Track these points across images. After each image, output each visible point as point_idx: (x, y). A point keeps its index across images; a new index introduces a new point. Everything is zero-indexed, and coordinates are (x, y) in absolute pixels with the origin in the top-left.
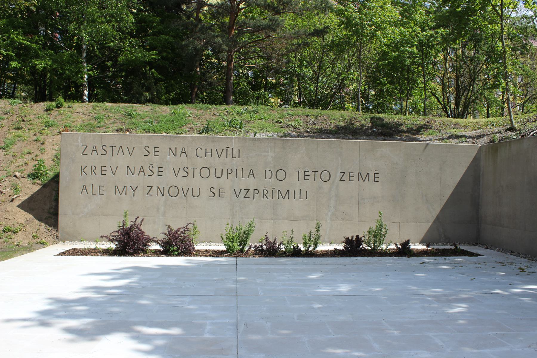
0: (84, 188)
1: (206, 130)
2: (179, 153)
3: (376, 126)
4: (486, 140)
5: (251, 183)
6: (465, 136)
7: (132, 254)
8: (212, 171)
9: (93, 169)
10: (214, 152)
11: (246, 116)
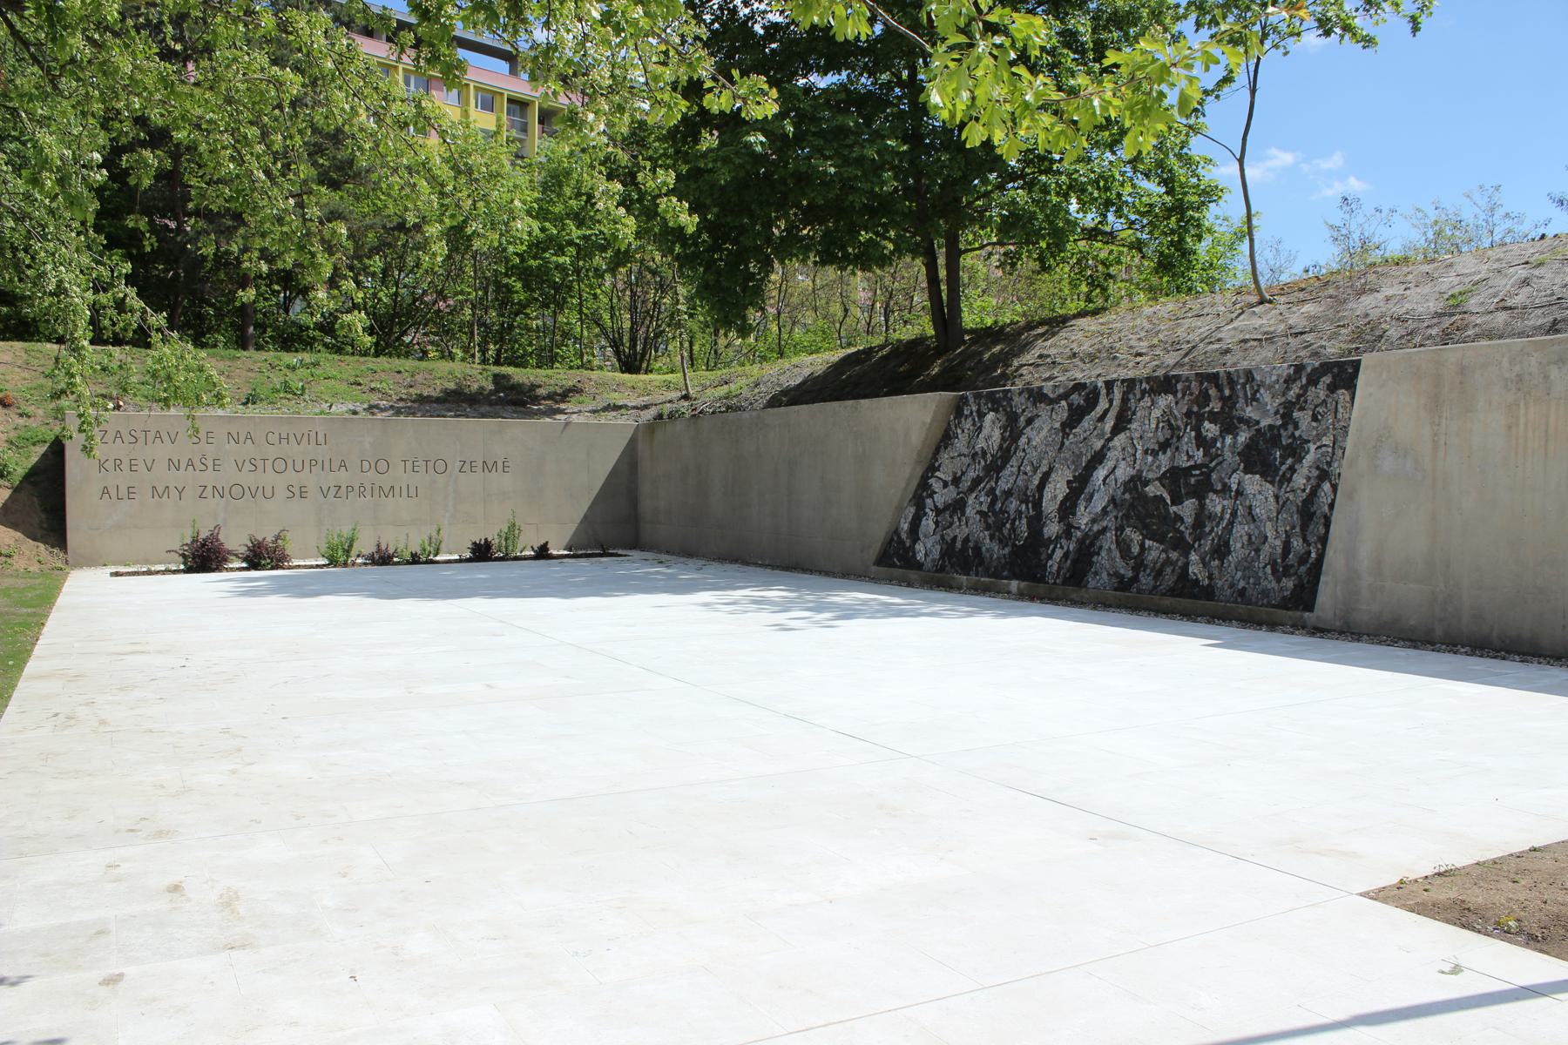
0: (105, 491)
1: (250, 400)
2: (242, 439)
3: (504, 389)
4: (653, 412)
5: (343, 477)
6: (625, 407)
7: (213, 571)
8: (290, 464)
9: (118, 465)
10: (292, 438)
11: (303, 372)
